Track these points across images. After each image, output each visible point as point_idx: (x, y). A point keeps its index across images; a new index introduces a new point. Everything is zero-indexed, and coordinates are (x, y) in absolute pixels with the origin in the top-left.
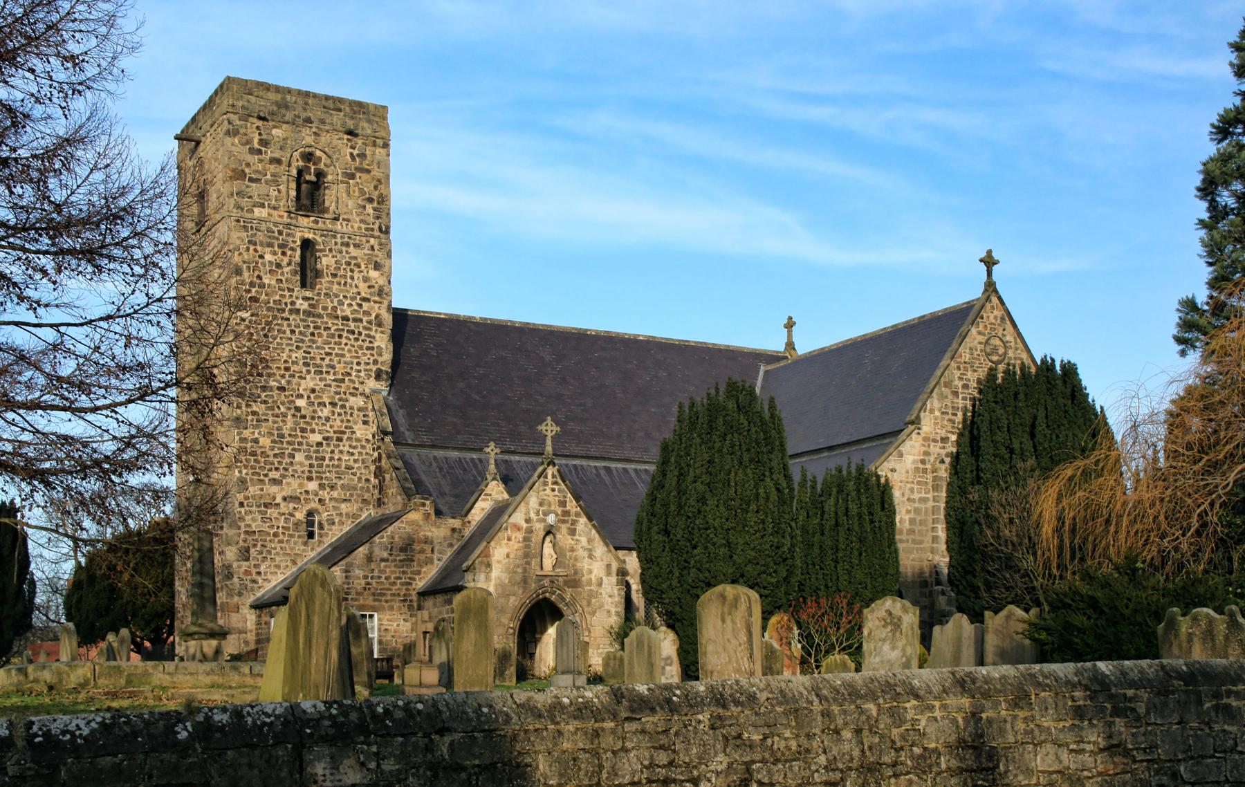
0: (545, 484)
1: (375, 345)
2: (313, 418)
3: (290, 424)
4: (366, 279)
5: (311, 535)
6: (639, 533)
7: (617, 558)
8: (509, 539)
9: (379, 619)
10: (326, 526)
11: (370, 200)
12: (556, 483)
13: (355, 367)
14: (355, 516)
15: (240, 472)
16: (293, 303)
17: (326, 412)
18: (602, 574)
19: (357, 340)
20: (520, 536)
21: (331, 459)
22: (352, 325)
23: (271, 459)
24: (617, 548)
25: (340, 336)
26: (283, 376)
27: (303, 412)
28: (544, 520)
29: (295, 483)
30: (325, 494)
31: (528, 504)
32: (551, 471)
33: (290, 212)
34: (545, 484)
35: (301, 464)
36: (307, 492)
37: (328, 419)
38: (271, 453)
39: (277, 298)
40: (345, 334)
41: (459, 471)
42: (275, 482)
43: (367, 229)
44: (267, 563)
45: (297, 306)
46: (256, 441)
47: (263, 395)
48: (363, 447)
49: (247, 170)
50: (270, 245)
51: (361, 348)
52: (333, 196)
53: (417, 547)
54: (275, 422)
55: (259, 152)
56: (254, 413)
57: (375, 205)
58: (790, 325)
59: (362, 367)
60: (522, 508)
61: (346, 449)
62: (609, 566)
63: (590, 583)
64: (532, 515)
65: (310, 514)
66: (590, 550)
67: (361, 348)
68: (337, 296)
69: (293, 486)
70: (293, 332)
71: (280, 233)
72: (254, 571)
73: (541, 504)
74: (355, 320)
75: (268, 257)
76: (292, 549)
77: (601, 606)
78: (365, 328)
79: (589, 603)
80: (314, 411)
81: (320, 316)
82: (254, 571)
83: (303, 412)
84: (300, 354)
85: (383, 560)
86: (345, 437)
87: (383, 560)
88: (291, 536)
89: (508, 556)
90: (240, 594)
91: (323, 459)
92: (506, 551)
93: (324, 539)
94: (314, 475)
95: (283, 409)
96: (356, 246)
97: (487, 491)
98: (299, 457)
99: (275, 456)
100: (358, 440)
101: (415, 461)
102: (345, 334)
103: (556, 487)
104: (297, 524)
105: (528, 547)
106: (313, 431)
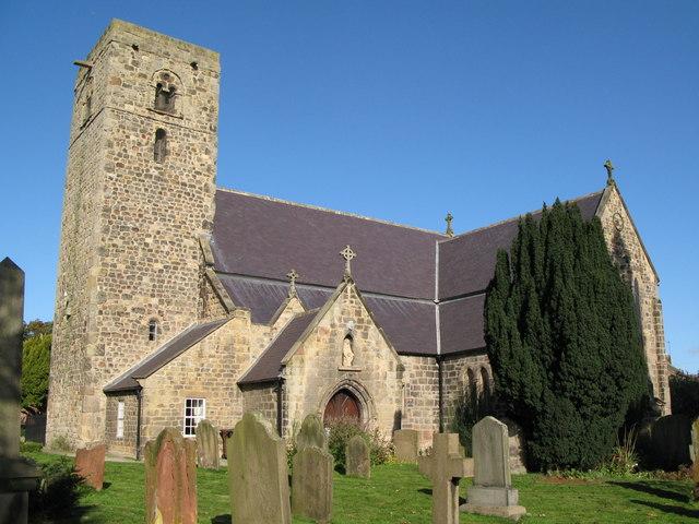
0: (346, 297)
1: (204, 204)
2: (157, 252)
4: (199, 160)
5: (151, 338)
6: (488, 339)
7: (399, 360)
9: (207, 404)
10: (163, 331)
11: (205, 109)
12: (353, 297)
13: (189, 218)
14: (185, 324)
16: (148, 170)
17: (167, 248)
18: (387, 369)
19: (191, 199)
20: (327, 337)
21: (169, 282)
22: (188, 190)
23: (125, 279)
24: (400, 353)
25: (179, 196)
26: (137, 221)
29: (141, 299)
30: (163, 308)
31: (333, 312)
32: (349, 287)
33: (150, 110)
34: (346, 297)
35: (147, 285)
36: (150, 305)
37: (168, 253)
39: (137, 165)
40: (183, 195)
41: (263, 295)
42: (127, 297)
43: (202, 127)
44: (119, 357)
45: (151, 172)
46: (115, 266)
47: (122, 233)
48: (192, 275)
49: (122, 79)
50: (133, 130)
51: (194, 205)
52: (182, 104)
53: (237, 346)
55: (132, 69)
56: (114, 245)
57: (208, 112)
58: (449, 219)
59: (193, 219)
60: (328, 315)
61: (180, 275)
62: (391, 363)
64: (336, 321)
65: (152, 321)
67: (194, 205)
68: (179, 168)
69: (139, 300)
70: (146, 190)
71: (142, 122)
72: (107, 364)
74: (191, 186)
75: (132, 138)
76: (137, 347)
78: (197, 192)
79: (377, 394)
81: (166, 181)
82: (107, 364)
84: (150, 206)
85: (210, 356)
86: (179, 267)
87: (210, 356)
88: (137, 337)
90: (96, 381)
91: (163, 281)
93: (161, 340)
94: (156, 293)
95: (135, 244)
96: (194, 137)
97: (290, 305)
98: (146, 279)
100: (189, 270)
101: (231, 284)
102: (183, 195)
104: (142, 329)
106: (157, 261)
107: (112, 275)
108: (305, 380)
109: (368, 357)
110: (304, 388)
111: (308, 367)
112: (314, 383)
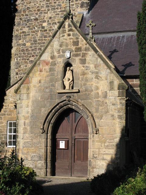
2: (50, 30)
3: (39, 34)
8: (41, 71)
12: (71, 30)
15: (17, 59)
20: (47, 68)
26: (37, 14)
27: (45, 28)
28: (63, 56)
31: (52, 46)
34: (64, 32)
38: (30, 49)
46: (24, 45)
54: (33, 35)
56: (23, 32)
62: (111, 83)
63: (97, 95)
64: (56, 54)
66: (97, 73)
73: (61, 46)
77: (107, 112)
79: (97, 111)
80: (51, 27)
83: (45, 28)
89: (40, 82)
92: (39, 78)
99: (32, 50)
103: (71, 33)
105: (52, 75)
107: (23, 50)
108: (30, 104)
109: (87, 80)
110: (30, 109)
111: (33, 93)
112: (37, 105)
